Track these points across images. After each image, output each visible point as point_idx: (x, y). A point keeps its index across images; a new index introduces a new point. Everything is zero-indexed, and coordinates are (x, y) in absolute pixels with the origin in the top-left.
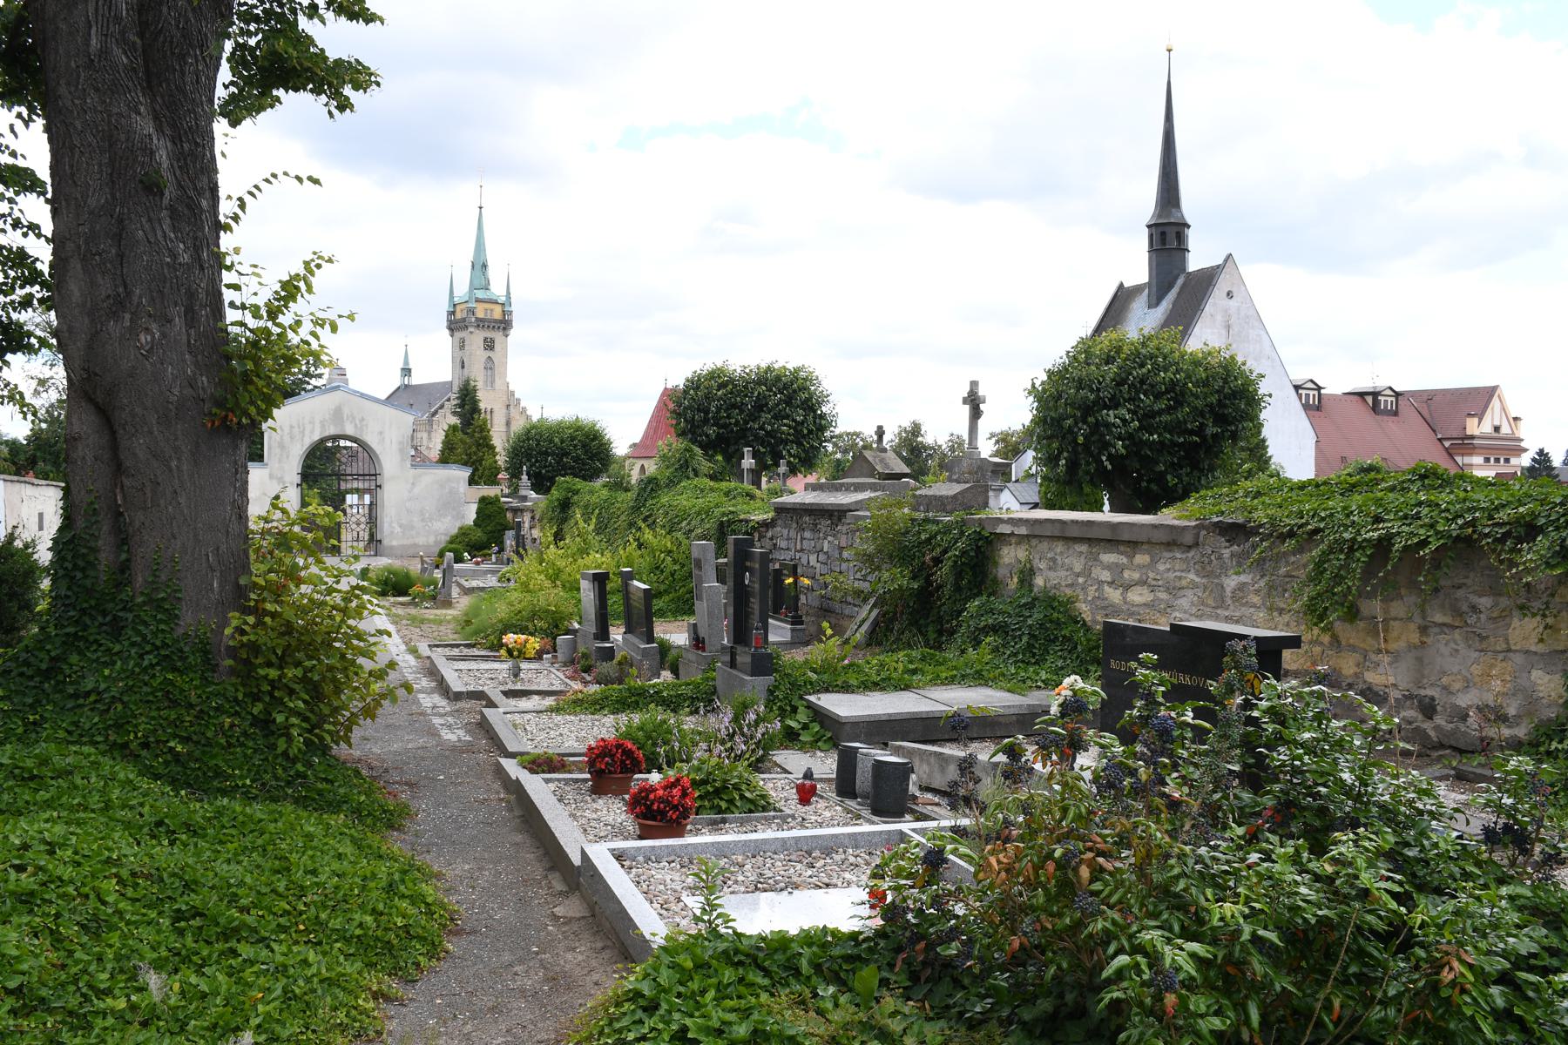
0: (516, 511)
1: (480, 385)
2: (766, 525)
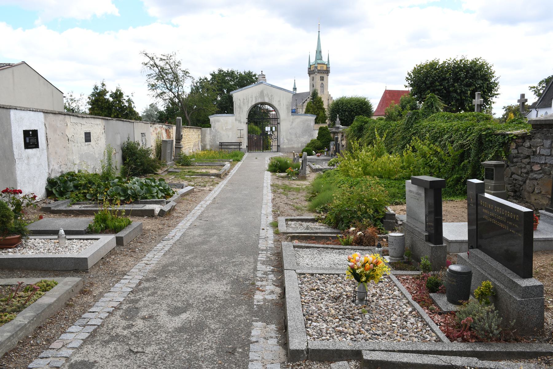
0: (335, 133)
1: (319, 92)
2: (524, 137)
